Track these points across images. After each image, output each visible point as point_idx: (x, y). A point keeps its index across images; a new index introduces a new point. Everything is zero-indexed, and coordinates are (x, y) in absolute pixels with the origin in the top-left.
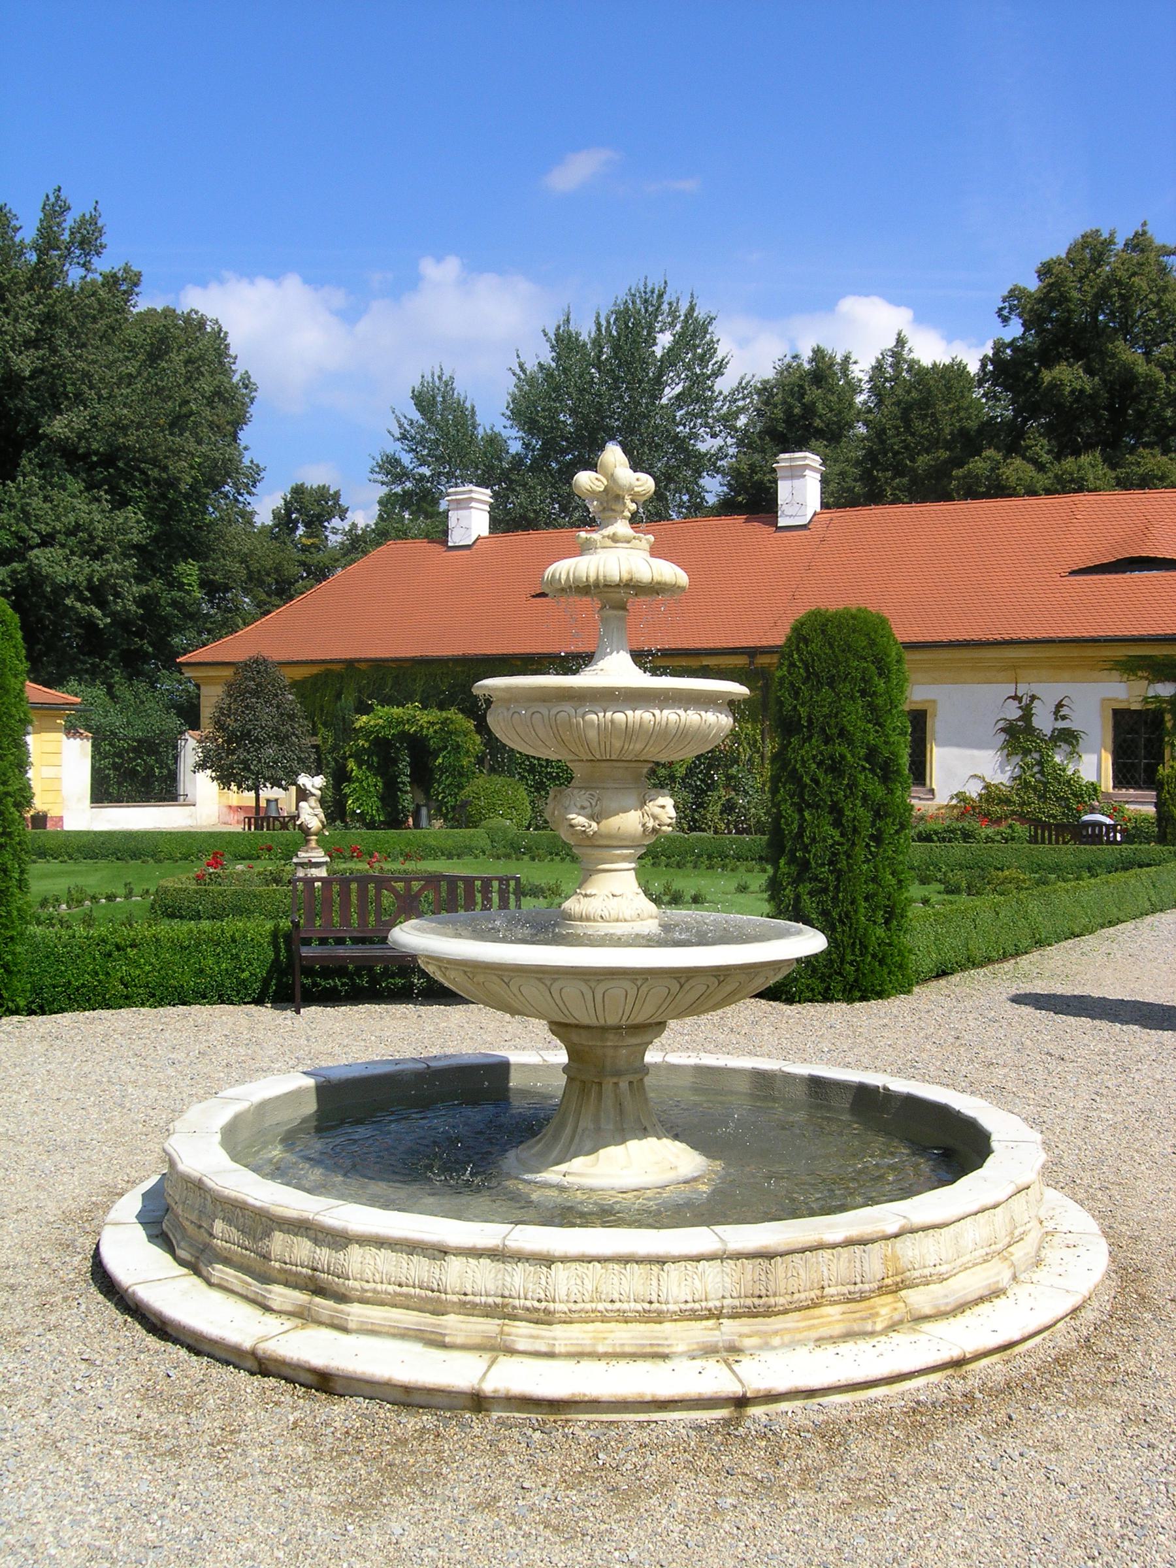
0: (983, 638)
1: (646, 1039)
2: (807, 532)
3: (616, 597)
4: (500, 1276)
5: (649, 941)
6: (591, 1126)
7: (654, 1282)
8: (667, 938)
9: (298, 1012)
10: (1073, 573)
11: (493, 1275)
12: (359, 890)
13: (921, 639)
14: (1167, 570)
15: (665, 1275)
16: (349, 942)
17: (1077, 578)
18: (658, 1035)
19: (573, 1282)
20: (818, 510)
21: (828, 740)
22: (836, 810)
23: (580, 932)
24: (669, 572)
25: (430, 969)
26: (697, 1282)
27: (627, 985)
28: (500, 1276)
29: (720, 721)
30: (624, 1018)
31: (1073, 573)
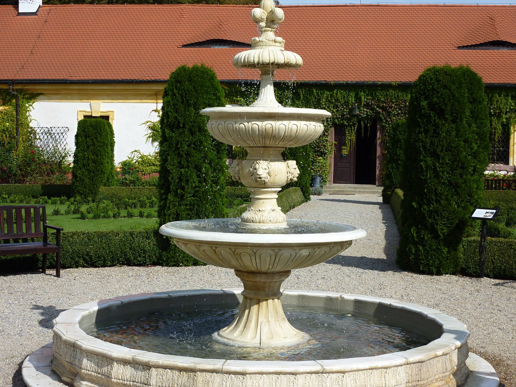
0: (145, 79)
1: (283, 278)
2: (36, 17)
3: (266, 68)
4: (320, 383)
5: (285, 232)
6: (265, 320)
7: (383, 379)
8: (295, 229)
9: (58, 275)
10: (184, 46)
11: (317, 384)
12: (16, 212)
13: (107, 78)
14: (220, 45)
15: (387, 375)
16: (20, 241)
17: (187, 49)
18: (288, 276)
19: (352, 382)
20: (41, 5)
21: (192, 133)
22: (198, 168)
23: (248, 227)
24: (294, 58)
25: (182, 247)
26: (398, 377)
27: (269, 251)
28: (320, 383)
29: (318, 128)
30: (270, 267)
31: (184, 46)
